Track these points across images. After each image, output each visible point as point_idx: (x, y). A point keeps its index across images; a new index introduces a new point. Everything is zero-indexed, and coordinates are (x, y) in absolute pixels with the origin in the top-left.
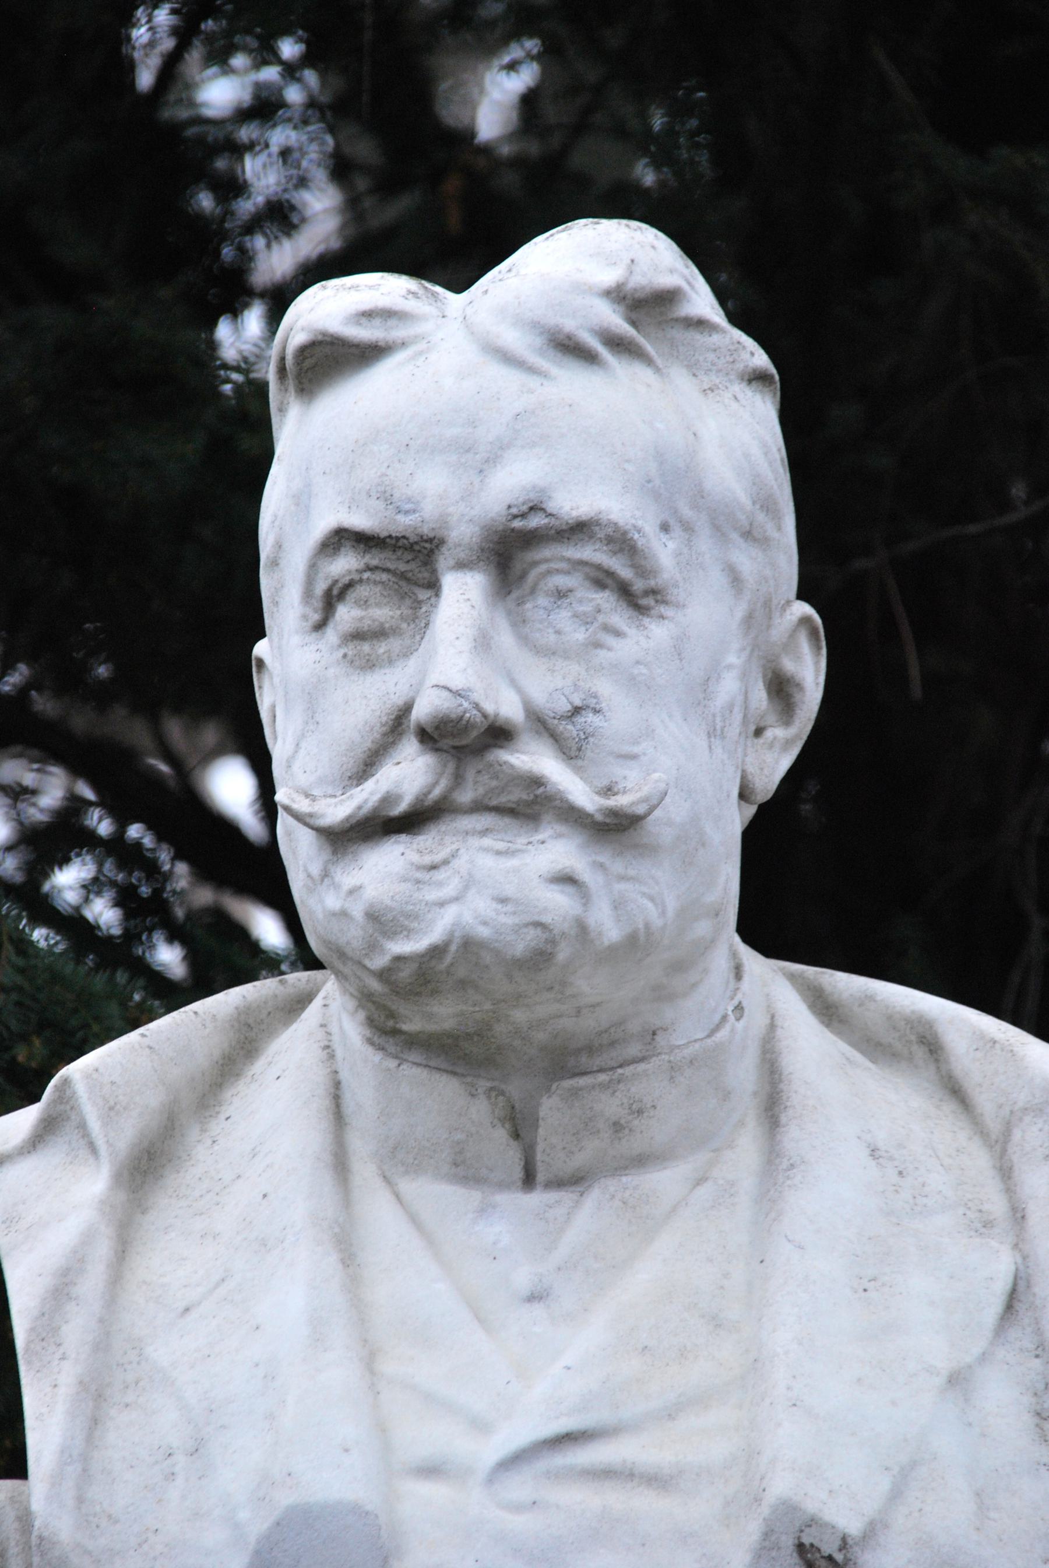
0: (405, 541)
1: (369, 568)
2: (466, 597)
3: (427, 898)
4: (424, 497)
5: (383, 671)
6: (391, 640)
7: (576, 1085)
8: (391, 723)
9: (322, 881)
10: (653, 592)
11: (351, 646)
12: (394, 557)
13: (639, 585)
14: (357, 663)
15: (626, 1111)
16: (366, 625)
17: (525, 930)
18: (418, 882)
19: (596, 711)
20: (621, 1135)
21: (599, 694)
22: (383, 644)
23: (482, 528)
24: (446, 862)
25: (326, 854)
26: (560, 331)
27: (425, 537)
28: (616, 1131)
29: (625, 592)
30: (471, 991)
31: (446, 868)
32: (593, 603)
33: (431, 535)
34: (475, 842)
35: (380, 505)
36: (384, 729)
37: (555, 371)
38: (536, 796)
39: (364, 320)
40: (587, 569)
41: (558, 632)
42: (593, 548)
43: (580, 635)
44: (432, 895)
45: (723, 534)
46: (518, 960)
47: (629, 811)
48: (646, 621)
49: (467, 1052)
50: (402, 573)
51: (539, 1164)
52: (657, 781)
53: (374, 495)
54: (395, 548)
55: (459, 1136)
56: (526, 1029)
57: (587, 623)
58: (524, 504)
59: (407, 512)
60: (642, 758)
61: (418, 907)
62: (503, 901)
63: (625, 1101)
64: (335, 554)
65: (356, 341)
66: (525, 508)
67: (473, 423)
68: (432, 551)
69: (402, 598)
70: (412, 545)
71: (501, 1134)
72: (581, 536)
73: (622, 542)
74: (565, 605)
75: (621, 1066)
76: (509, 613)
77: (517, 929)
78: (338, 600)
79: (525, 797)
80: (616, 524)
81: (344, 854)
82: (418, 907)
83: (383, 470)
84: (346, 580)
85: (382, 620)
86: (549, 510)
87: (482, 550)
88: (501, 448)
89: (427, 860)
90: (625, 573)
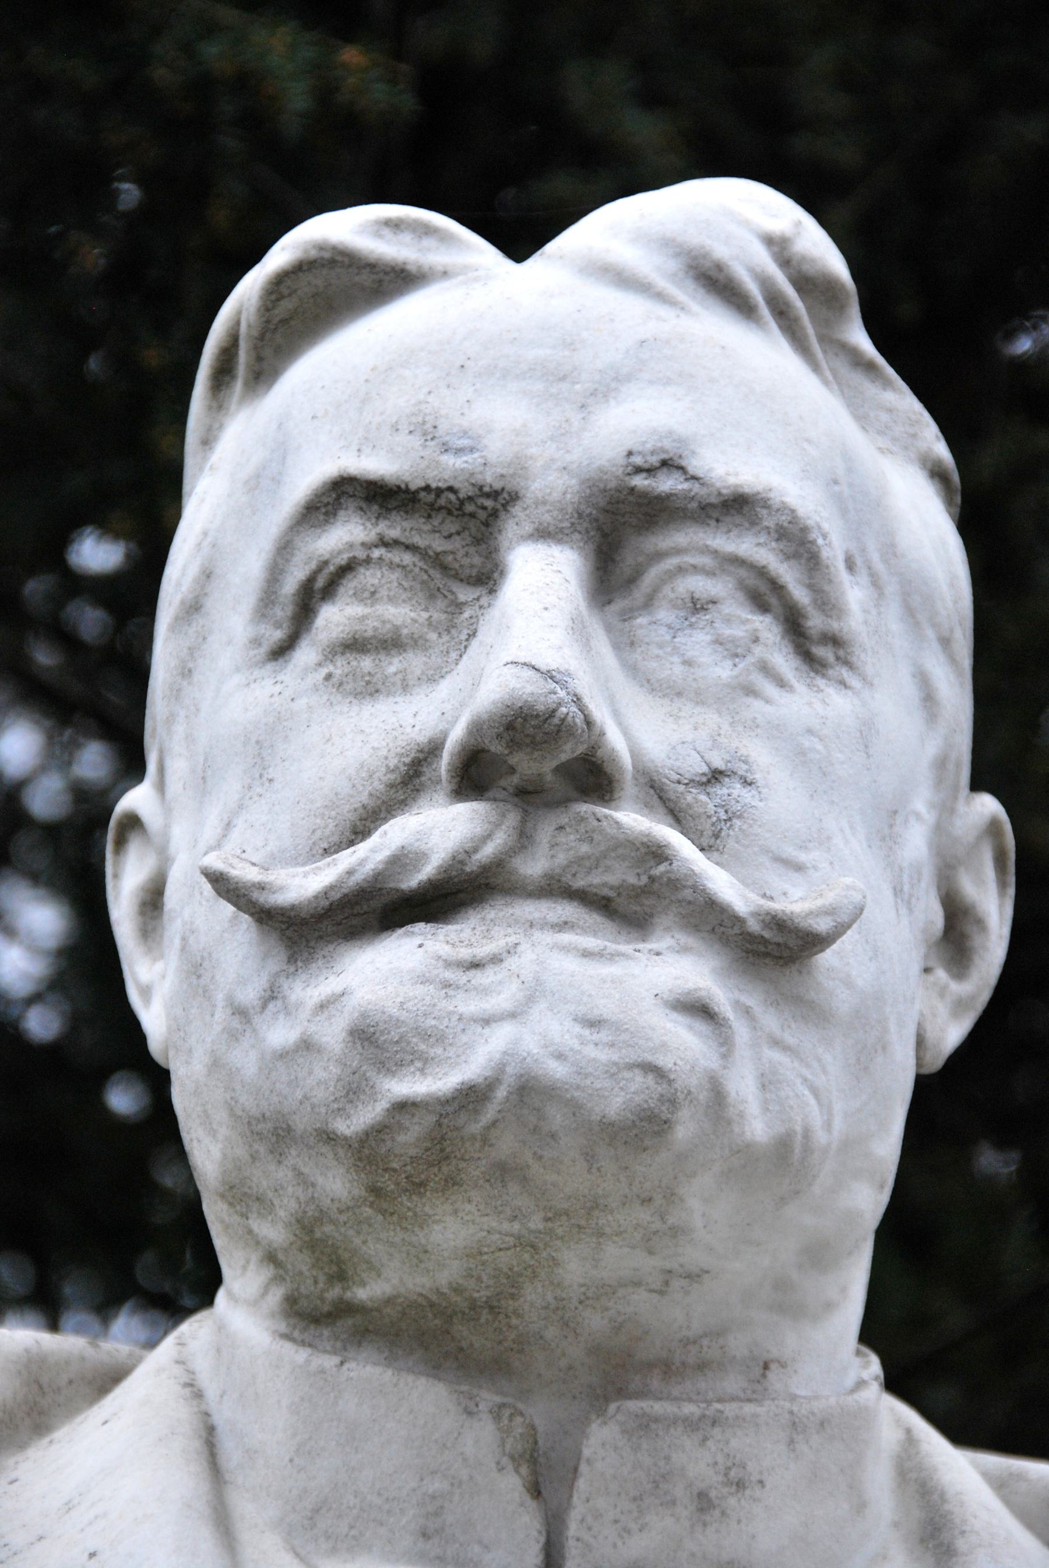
0: (452, 497)
1: (383, 542)
2: (555, 568)
3: (462, 1009)
4: (490, 431)
5: (391, 699)
6: (410, 655)
7: (648, 1410)
8: (403, 768)
9: (264, 1007)
10: (835, 641)
11: (340, 661)
12: (427, 527)
13: (815, 622)
14: (348, 687)
15: (721, 1478)
16: (369, 628)
17: (627, 1074)
18: (447, 985)
19: (747, 783)
20: (708, 1518)
21: (751, 760)
22: (396, 660)
23: (582, 483)
24: (496, 959)
25: (276, 962)
26: (706, 256)
27: (487, 489)
28: (701, 1510)
29: (794, 625)
30: (514, 1188)
31: (497, 969)
32: (748, 627)
33: (498, 486)
34: (549, 938)
35: (416, 441)
36: (392, 777)
37: (695, 307)
38: (652, 879)
39: (386, 231)
40: (743, 572)
41: (688, 663)
42: (755, 541)
43: (724, 671)
44: (470, 1005)
45: (917, 624)
46: (612, 1124)
47: (803, 924)
48: (820, 682)
49: (464, 1344)
50: (437, 554)
51: (571, 1543)
52: (848, 888)
53: (404, 428)
54: (432, 509)
55: (437, 1485)
56: (575, 1302)
57: (737, 655)
58: (652, 453)
59: (459, 451)
60: (811, 872)
61: (446, 1022)
62: (594, 1023)
63: (720, 1459)
64: (327, 521)
65: (372, 258)
66: (654, 460)
67: (570, 344)
68: (494, 514)
69: (432, 597)
70: (462, 502)
71: (511, 1485)
72: (738, 519)
73: (797, 540)
74: (702, 624)
75: (720, 1400)
76: (609, 629)
77: (614, 1071)
78: (323, 599)
79: (632, 880)
80: (793, 511)
81: (307, 962)
82: (446, 1022)
83: (421, 397)
84: (343, 559)
85: (399, 622)
86: (691, 470)
87: (580, 516)
88: (616, 379)
89: (465, 953)
90: (800, 595)
